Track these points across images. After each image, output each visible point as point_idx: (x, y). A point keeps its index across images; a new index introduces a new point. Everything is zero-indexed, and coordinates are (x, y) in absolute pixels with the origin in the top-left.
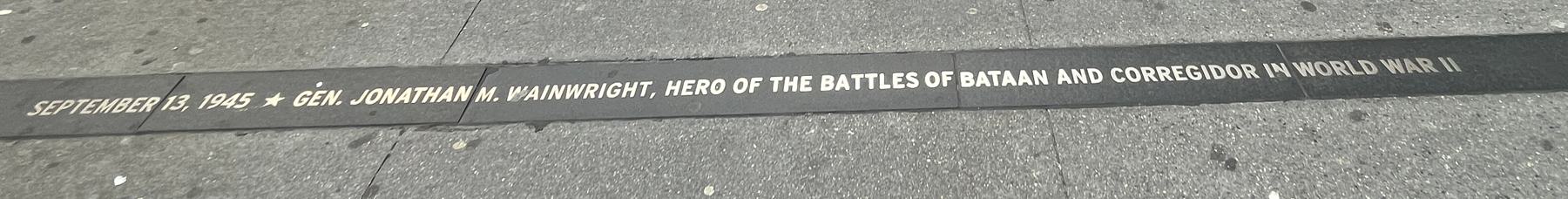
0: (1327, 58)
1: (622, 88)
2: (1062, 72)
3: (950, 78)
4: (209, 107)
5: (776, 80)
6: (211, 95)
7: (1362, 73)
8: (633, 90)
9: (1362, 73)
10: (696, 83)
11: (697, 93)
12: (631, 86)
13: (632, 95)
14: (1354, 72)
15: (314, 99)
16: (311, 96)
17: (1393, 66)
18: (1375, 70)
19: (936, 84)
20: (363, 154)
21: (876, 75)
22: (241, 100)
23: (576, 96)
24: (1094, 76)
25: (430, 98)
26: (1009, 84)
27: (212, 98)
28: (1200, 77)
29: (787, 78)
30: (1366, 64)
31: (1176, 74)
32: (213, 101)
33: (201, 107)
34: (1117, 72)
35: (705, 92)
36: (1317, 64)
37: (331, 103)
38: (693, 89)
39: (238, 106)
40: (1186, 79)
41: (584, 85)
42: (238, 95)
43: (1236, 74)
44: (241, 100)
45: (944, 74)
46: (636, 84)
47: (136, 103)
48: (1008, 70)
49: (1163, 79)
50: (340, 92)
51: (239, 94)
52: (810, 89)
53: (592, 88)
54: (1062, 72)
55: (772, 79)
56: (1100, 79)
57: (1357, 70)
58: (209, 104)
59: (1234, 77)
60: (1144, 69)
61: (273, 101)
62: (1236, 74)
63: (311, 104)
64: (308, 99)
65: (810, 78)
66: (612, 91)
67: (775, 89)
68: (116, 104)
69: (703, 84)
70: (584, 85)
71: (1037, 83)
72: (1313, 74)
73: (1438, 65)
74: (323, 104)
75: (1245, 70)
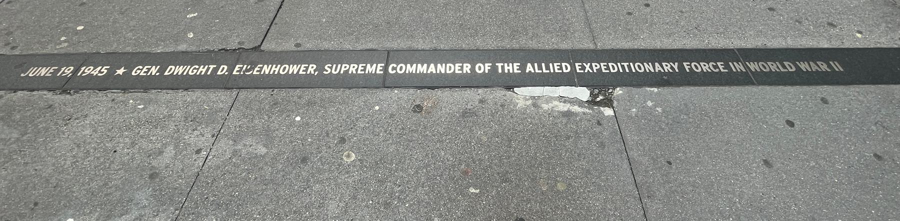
0: (766, 60)
1: (198, 69)
2: (529, 65)
3: (490, 68)
4: (84, 75)
5: (499, 65)
6: (85, 67)
7: (786, 70)
8: (204, 70)
9: (786, 70)
10: (309, 66)
11: (308, 73)
12: (204, 68)
13: (203, 74)
14: (783, 70)
15: (143, 71)
16: (142, 69)
17: (804, 66)
18: (794, 69)
19: (482, 71)
20: (806, 151)
21: (502, 64)
22: (102, 71)
23: (295, 73)
24: (566, 68)
25: (275, 71)
26: (530, 71)
27: (66, 69)
28: (616, 70)
29: (369, 65)
30: (762, 65)
31: (603, 68)
32: (86, 71)
33: (79, 75)
34: (713, 65)
35: (354, 72)
36: (760, 63)
37: (153, 74)
38: (306, 71)
39: (99, 75)
40: (561, 71)
41: (299, 66)
42: (100, 67)
43: (639, 66)
44: (102, 71)
45: (487, 65)
46: (207, 66)
47: (145, 70)
48: (369, 63)
49: (666, 71)
50: (158, 67)
51: (101, 67)
52: (382, 72)
53: (354, 67)
54: (529, 65)
55: (497, 64)
56: (569, 70)
57: (715, 69)
58: (84, 72)
59: (640, 71)
60: (702, 64)
61: (121, 71)
62: (639, 66)
63: (142, 74)
64: (196, 70)
65: (519, 64)
66: (191, 71)
67: (500, 71)
68: (48, 71)
69: (467, 67)
70: (299, 66)
71: (438, 72)
72: (759, 70)
73: (829, 66)
74: (149, 74)
75: (771, 66)
